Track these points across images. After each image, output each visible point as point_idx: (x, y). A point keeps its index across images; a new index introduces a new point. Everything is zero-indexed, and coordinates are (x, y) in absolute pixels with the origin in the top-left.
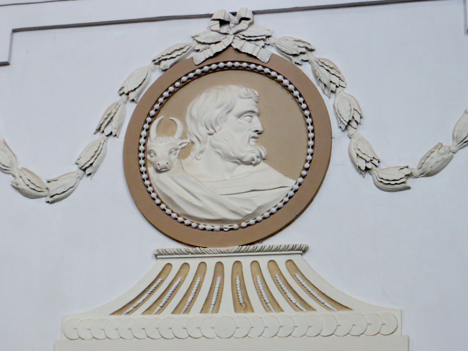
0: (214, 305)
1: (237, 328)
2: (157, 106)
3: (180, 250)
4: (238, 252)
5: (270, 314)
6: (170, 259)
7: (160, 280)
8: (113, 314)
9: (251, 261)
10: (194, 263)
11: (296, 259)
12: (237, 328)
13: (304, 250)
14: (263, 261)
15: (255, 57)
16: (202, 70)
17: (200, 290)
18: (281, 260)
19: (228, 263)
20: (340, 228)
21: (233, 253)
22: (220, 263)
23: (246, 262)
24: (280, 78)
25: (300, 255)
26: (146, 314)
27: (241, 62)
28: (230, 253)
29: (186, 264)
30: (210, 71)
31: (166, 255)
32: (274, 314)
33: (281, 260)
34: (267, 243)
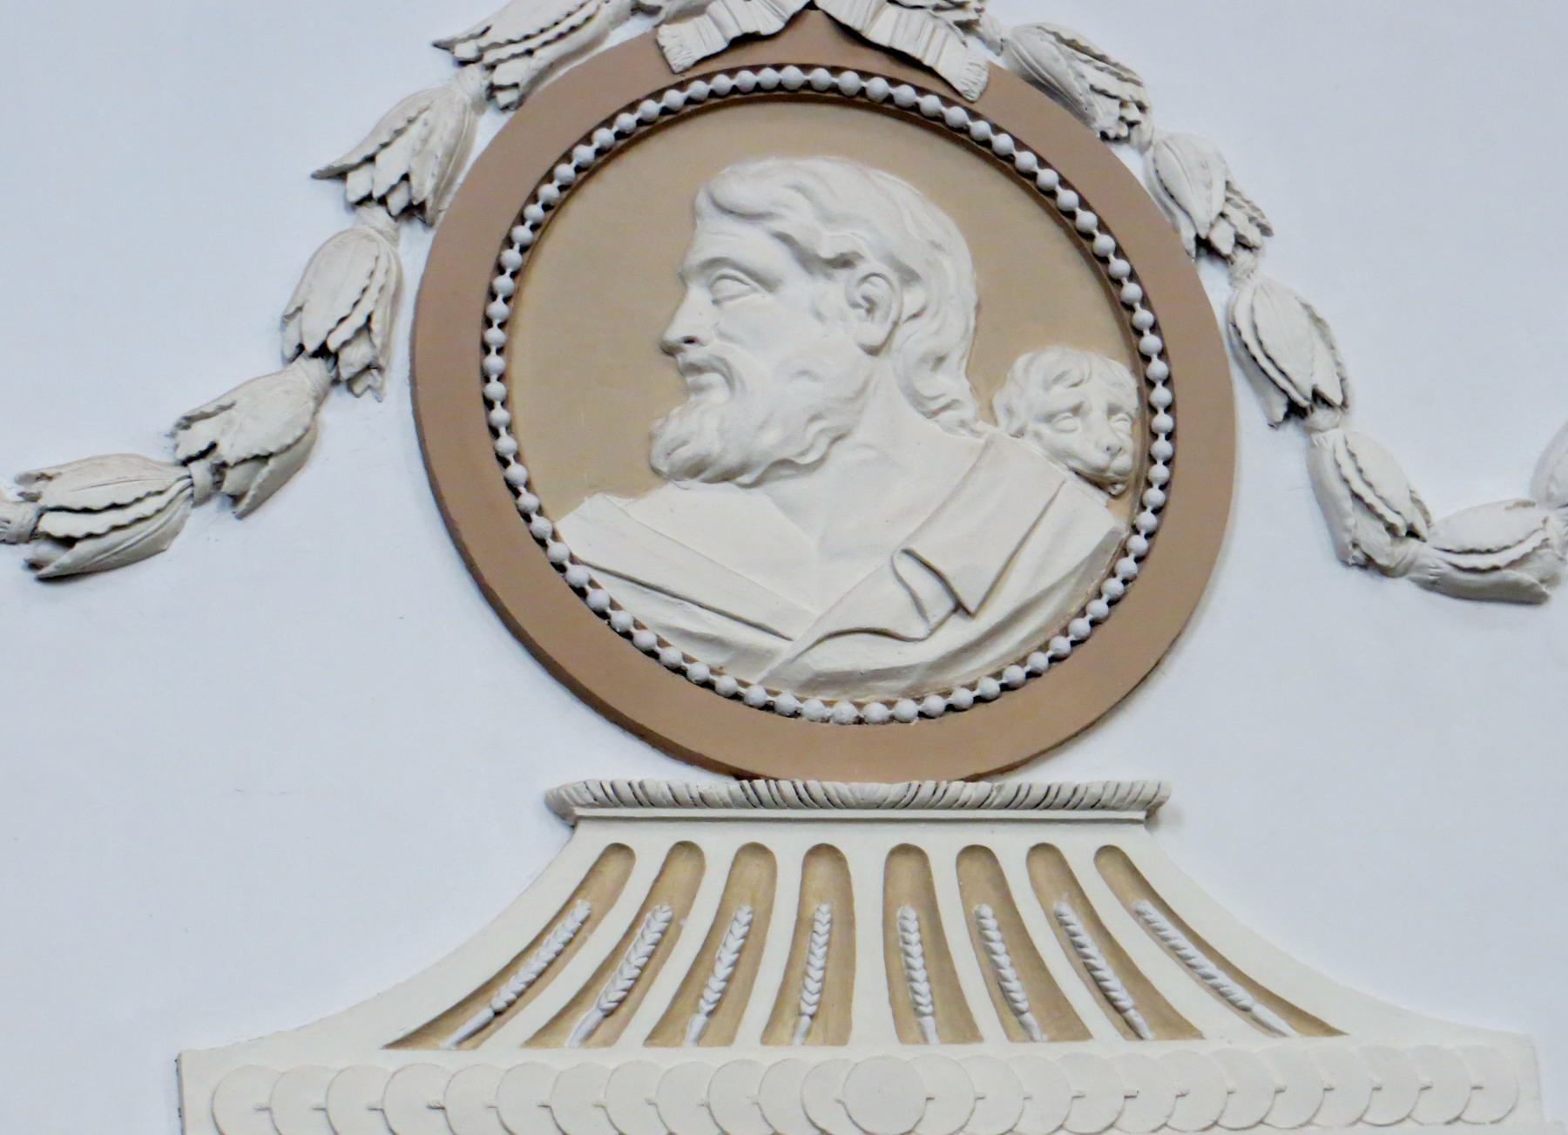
0: (710, 1014)
1: (1475, 1088)
2: (550, 191)
3: (641, 785)
4: (906, 806)
5: (1024, 1049)
6: (1045, 827)
7: (581, 910)
8: (1330, 1031)
9: (1033, 844)
10: (719, 845)
11: (1132, 841)
12: (1475, 1088)
13: (1151, 810)
14: (1011, 845)
15: (930, 71)
16: (944, 109)
17: (669, 952)
18: (1078, 845)
19: (866, 850)
20: (1268, 735)
21: (1085, 808)
22: (757, 849)
23: (942, 845)
24: (1025, 160)
25: (1141, 829)
26: (546, 1046)
27: (865, 75)
28: (963, 806)
29: (619, 848)
30: (859, 99)
31: (641, 804)
32: (938, 1050)
33: (1078, 845)
34: (1039, 778)
